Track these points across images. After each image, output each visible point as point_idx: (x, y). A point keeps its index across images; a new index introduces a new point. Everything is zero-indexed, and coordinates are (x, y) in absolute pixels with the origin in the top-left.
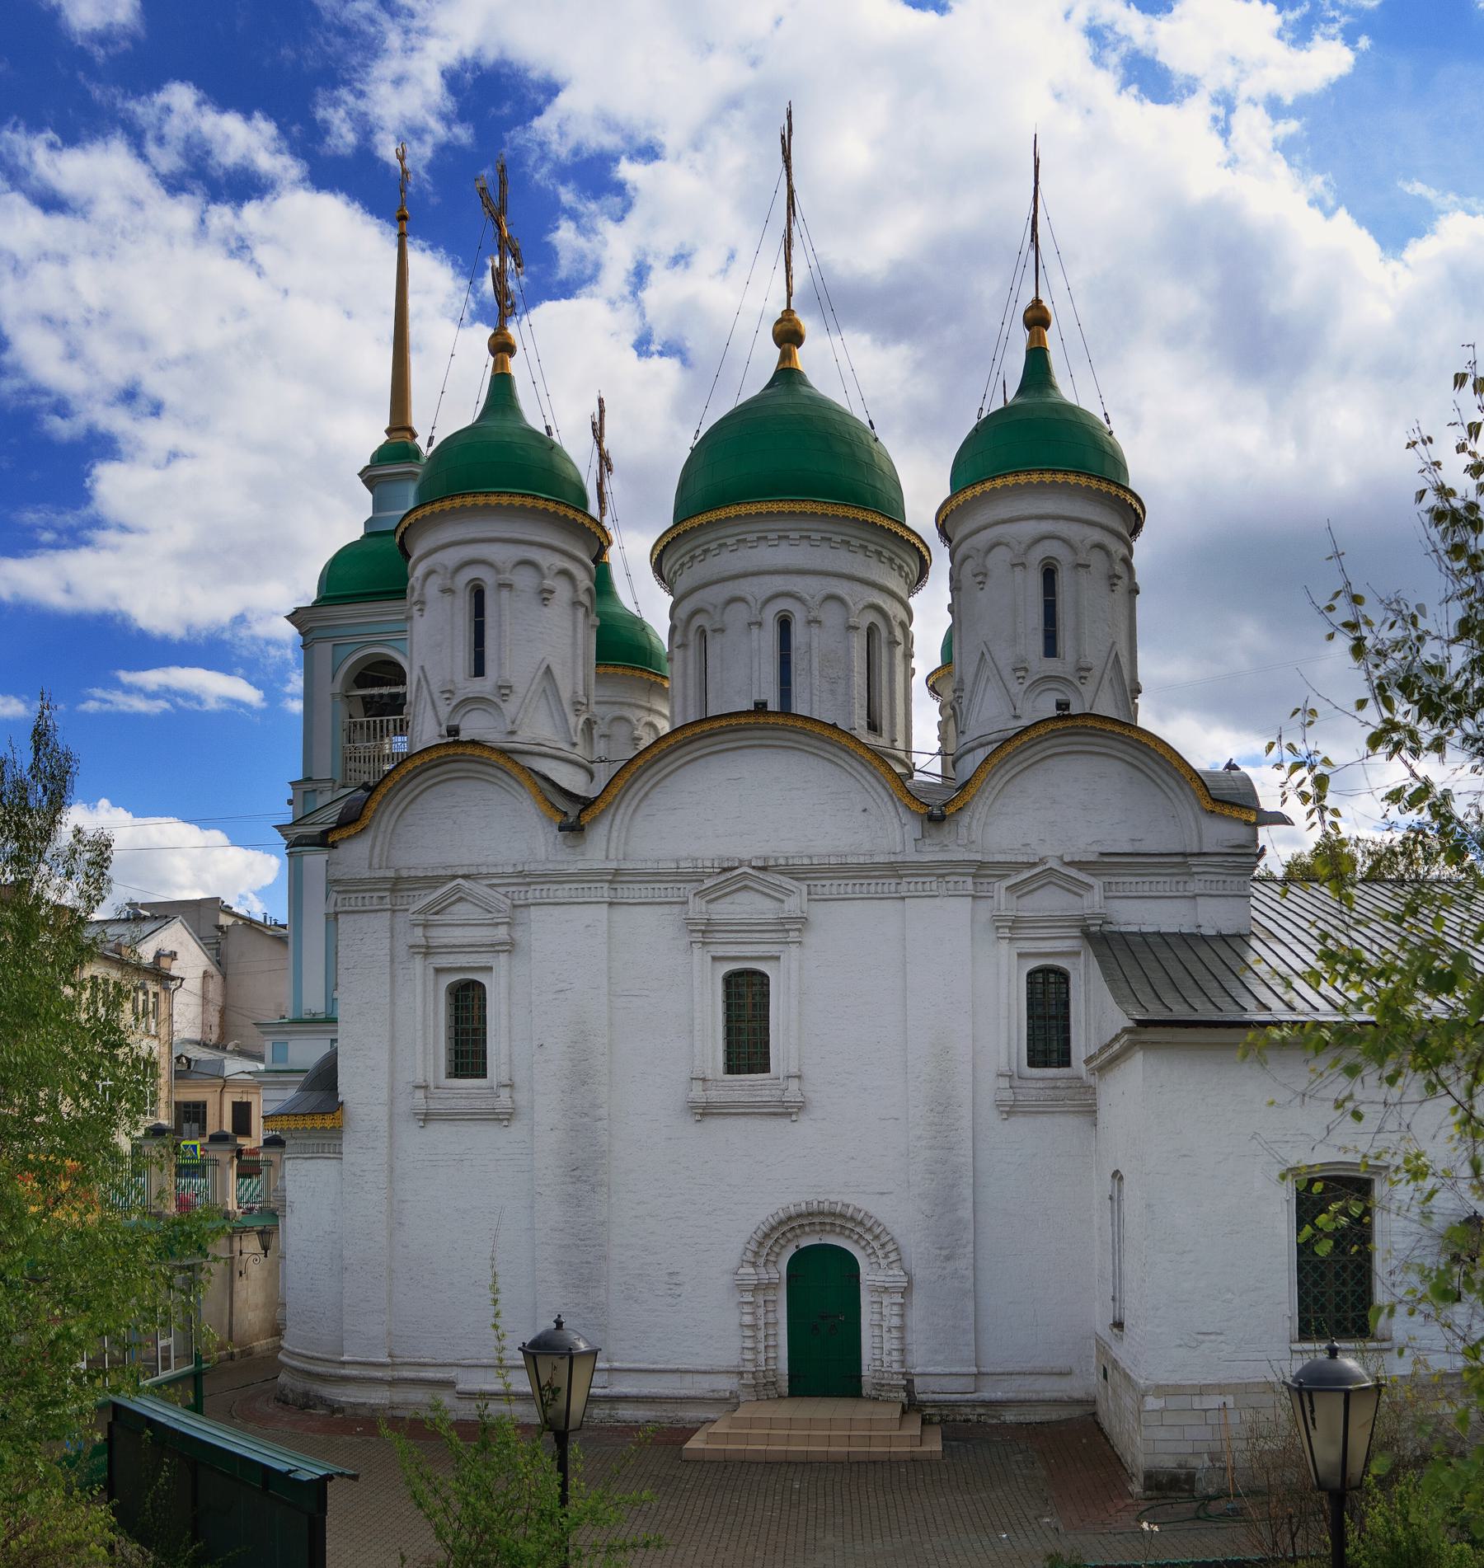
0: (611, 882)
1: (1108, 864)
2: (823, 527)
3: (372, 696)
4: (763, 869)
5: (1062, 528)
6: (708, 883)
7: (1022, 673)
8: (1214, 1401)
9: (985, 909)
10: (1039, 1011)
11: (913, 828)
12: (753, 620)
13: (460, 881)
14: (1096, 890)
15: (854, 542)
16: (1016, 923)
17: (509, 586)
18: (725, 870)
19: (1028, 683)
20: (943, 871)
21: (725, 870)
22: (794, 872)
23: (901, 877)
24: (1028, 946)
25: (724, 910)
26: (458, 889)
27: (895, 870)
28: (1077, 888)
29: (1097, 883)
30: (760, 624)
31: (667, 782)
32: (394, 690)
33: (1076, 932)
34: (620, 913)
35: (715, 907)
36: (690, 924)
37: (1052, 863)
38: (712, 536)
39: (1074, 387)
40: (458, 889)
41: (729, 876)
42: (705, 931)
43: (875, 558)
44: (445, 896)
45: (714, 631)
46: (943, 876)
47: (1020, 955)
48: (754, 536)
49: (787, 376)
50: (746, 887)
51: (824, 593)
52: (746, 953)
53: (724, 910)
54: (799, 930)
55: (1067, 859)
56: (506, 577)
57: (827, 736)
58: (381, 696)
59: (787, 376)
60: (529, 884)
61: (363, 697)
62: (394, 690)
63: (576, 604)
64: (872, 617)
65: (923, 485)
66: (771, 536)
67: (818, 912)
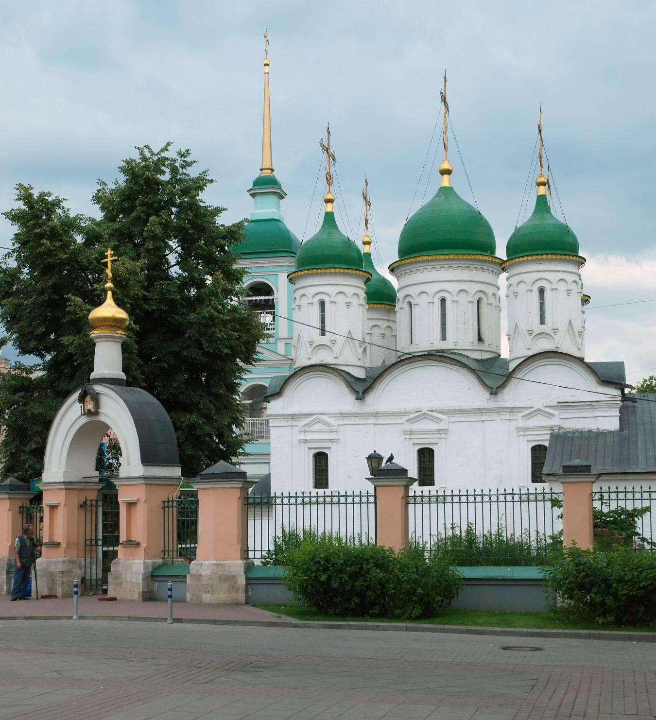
0: (374, 416)
1: (564, 405)
2: (458, 262)
5: (542, 275)
6: (412, 416)
7: (531, 332)
11: (486, 394)
14: (556, 416)
15: (471, 266)
16: (526, 429)
18: (417, 412)
19: (533, 336)
21: (417, 412)
23: (483, 413)
24: (530, 438)
25: (416, 427)
26: (317, 418)
27: (480, 411)
30: (433, 303)
32: (267, 298)
34: (378, 428)
36: (405, 432)
37: (541, 407)
41: (421, 416)
43: (481, 270)
44: (313, 421)
45: (415, 305)
46: (498, 412)
47: (528, 441)
48: (430, 267)
50: (425, 418)
51: (459, 289)
52: (426, 441)
53: (416, 427)
55: (545, 405)
58: (260, 300)
61: (250, 301)
62: (267, 298)
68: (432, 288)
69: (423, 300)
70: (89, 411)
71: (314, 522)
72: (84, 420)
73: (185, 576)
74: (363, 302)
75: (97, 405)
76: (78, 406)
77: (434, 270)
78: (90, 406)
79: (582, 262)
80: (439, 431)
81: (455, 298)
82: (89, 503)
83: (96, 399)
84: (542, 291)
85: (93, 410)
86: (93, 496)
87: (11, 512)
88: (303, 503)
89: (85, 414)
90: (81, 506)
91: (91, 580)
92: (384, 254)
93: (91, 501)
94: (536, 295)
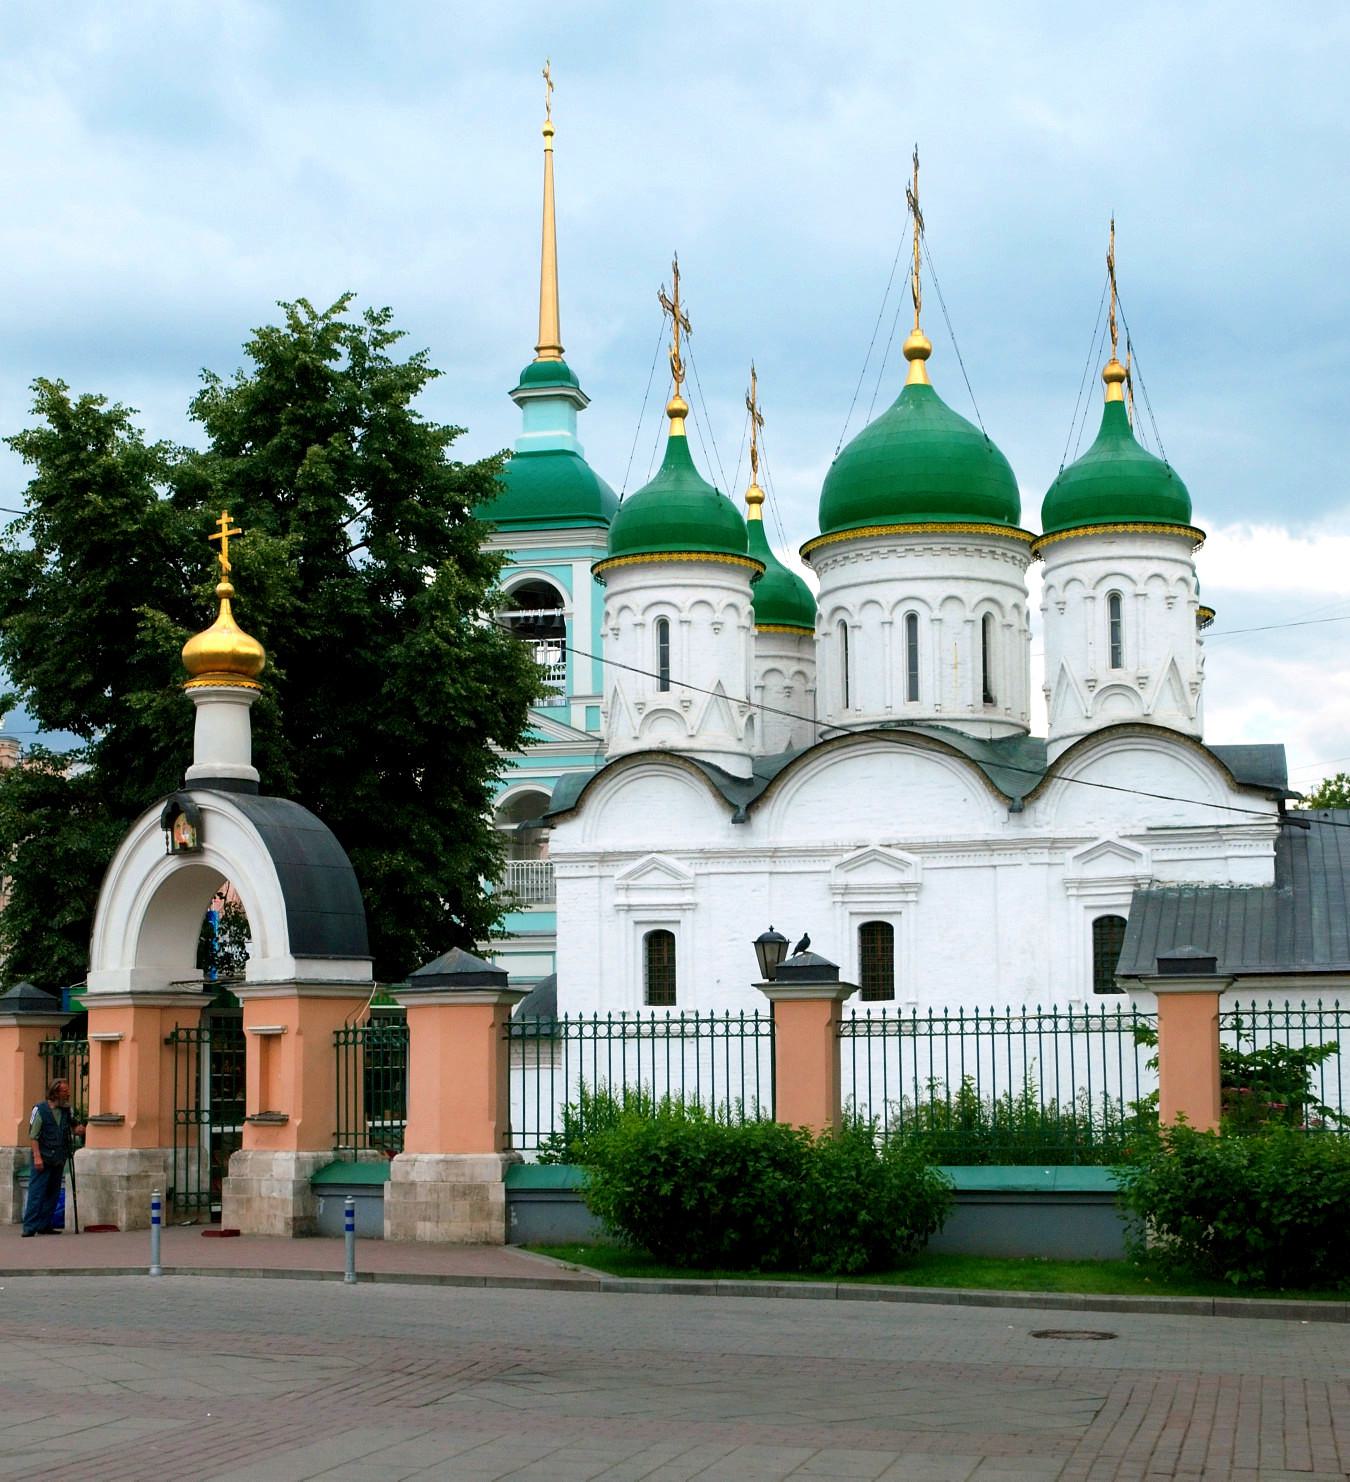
0: (771, 857)
1: (1159, 834)
2: (942, 540)
3: (518, 618)
4: (889, 846)
6: (847, 856)
9: (1058, 874)
10: (1099, 950)
11: (1000, 812)
12: (887, 620)
13: (654, 855)
15: (970, 548)
16: (1082, 883)
17: (688, 622)
18: (859, 847)
19: (1097, 690)
21: (859, 847)
23: (993, 850)
24: (1090, 901)
25: (856, 878)
26: (653, 861)
27: (988, 846)
31: (813, 780)
37: (1114, 838)
38: (852, 548)
40: (653, 861)
41: (866, 855)
43: (989, 556)
44: (644, 866)
45: (853, 627)
47: (1086, 907)
50: (875, 860)
52: (877, 909)
53: (856, 878)
54: (916, 892)
58: (536, 618)
60: (709, 858)
61: (515, 620)
66: (899, 549)
67: (932, 880)
68: (888, 594)
70: (184, 845)
71: (646, 1074)
72: (173, 864)
73: (381, 1187)
74: (747, 621)
75: (200, 835)
76: (160, 835)
77: (892, 557)
78: (186, 836)
79: (1197, 538)
80: (903, 887)
81: (937, 614)
82: (182, 1035)
83: (197, 820)
84: (1115, 599)
85: (191, 845)
88: (624, 1036)
89: (174, 852)
90: (167, 1042)
91: (187, 1194)
92: (789, 522)
93: (188, 1031)
94: (1103, 608)
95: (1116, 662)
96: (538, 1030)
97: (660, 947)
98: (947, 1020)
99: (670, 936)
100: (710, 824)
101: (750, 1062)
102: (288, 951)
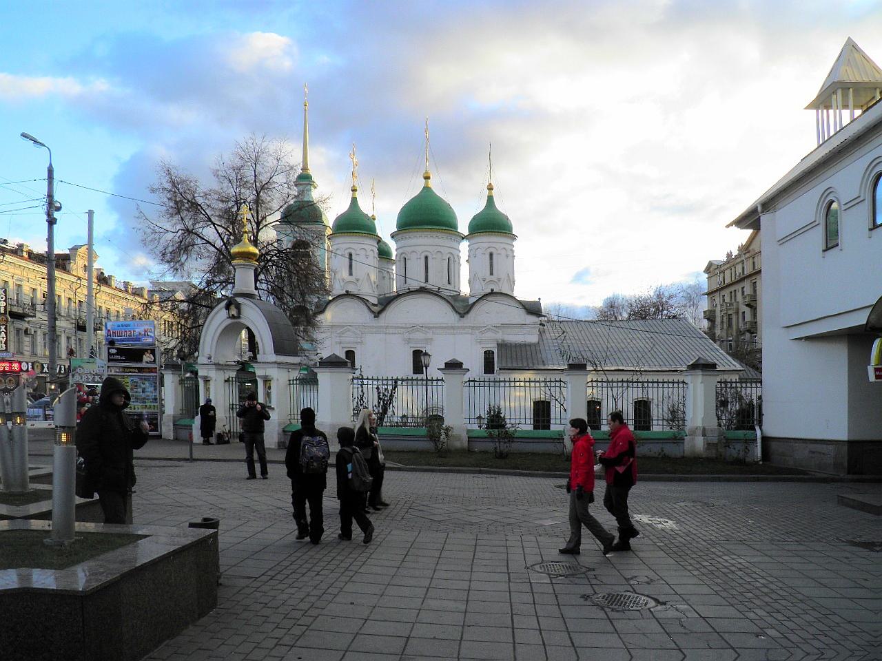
1: (504, 326)
8: (136, 417)
11: (457, 316)
20: (463, 328)
22: (429, 328)
25: (412, 336)
28: (496, 332)
29: (500, 331)
33: (496, 343)
35: (411, 335)
39: (501, 206)
41: (414, 328)
42: (409, 341)
49: (427, 189)
53: (412, 336)
56: (358, 252)
57: (436, 293)
59: (427, 189)
63: (374, 257)
64: (449, 255)
65: (463, 229)
68: (420, 249)
69: (413, 256)
70: (233, 315)
71: (440, 400)
72: (230, 321)
73: (191, 426)
74: (376, 256)
75: (239, 312)
76: (224, 312)
77: (420, 238)
78: (234, 312)
79: (514, 237)
80: (427, 340)
81: (434, 256)
82: (231, 379)
83: (238, 307)
84: (491, 255)
85: (236, 315)
86: (233, 374)
87: (703, 384)
88: (293, 384)
89: (229, 317)
90: (226, 381)
91: (234, 432)
92: (386, 227)
93: (232, 378)
94: (488, 257)
95: (491, 274)
96: (430, 380)
97: (417, 354)
98: (510, 381)
99: (353, 352)
100: (450, 317)
101: (482, 395)
102: (273, 352)
